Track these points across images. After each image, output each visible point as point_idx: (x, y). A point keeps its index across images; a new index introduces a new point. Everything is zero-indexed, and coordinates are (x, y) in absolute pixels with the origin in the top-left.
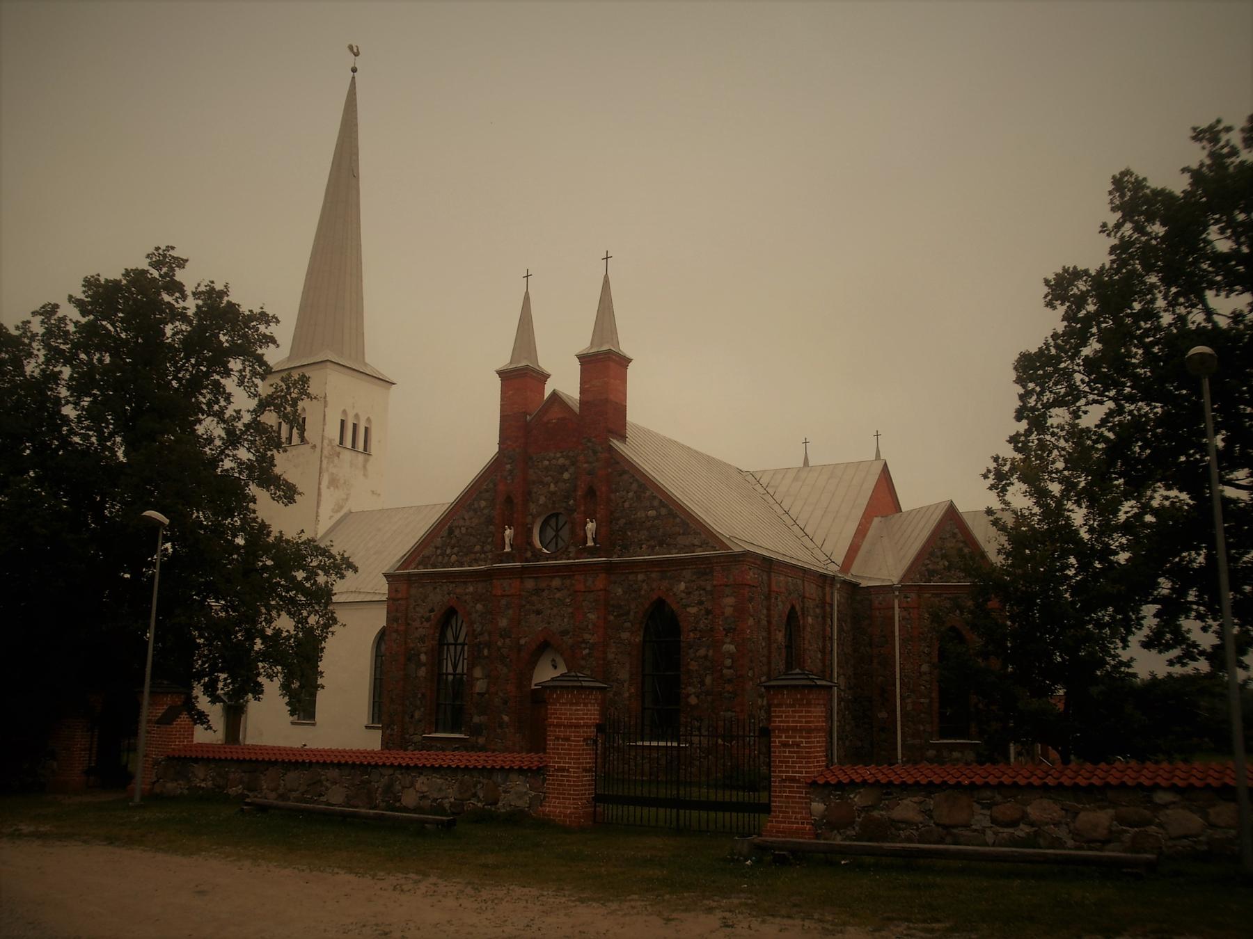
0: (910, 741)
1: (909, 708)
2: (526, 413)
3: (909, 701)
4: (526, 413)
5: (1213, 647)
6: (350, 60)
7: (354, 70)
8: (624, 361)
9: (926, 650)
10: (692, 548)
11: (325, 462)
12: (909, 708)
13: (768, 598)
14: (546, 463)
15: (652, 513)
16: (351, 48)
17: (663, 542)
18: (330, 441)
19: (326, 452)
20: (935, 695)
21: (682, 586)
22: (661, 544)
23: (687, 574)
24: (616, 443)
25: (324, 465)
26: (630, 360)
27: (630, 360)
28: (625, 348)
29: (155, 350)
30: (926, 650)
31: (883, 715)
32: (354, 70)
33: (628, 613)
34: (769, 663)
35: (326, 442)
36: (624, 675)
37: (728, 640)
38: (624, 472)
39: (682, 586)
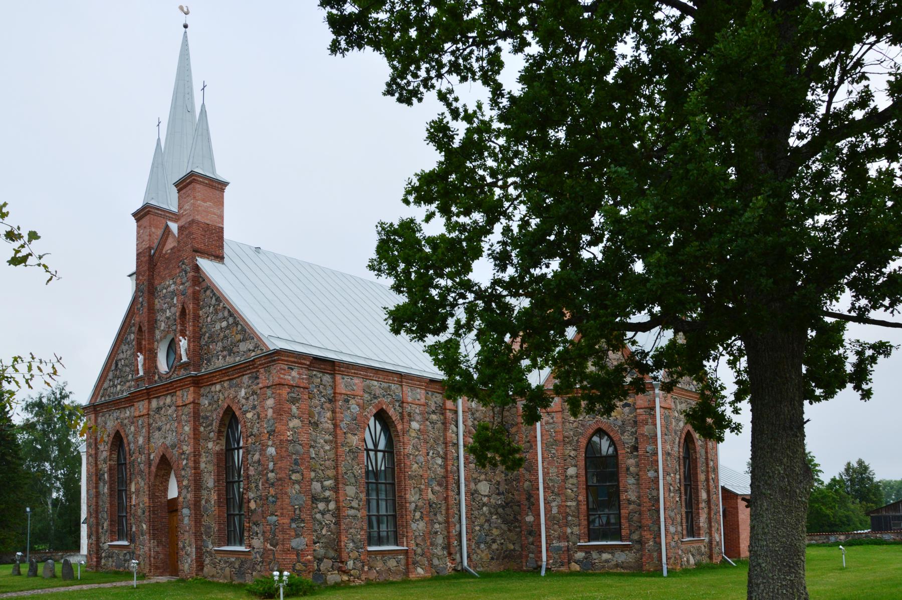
0: (556, 544)
1: (555, 511)
3: (554, 504)
5: (530, 384)
6: (183, 19)
7: (186, 26)
8: (219, 186)
9: (573, 453)
12: (555, 511)
13: (332, 400)
14: (165, 291)
15: (224, 324)
16: (181, 8)
20: (581, 498)
21: (243, 392)
23: (245, 379)
24: (206, 265)
26: (225, 184)
27: (225, 184)
30: (573, 453)
31: (530, 518)
32: (186, 26)
33: (211, 424)
34: (336, 468)
36: (211, 484)
37: (270, 443)
38: (208, 288)
39: (243, 392)
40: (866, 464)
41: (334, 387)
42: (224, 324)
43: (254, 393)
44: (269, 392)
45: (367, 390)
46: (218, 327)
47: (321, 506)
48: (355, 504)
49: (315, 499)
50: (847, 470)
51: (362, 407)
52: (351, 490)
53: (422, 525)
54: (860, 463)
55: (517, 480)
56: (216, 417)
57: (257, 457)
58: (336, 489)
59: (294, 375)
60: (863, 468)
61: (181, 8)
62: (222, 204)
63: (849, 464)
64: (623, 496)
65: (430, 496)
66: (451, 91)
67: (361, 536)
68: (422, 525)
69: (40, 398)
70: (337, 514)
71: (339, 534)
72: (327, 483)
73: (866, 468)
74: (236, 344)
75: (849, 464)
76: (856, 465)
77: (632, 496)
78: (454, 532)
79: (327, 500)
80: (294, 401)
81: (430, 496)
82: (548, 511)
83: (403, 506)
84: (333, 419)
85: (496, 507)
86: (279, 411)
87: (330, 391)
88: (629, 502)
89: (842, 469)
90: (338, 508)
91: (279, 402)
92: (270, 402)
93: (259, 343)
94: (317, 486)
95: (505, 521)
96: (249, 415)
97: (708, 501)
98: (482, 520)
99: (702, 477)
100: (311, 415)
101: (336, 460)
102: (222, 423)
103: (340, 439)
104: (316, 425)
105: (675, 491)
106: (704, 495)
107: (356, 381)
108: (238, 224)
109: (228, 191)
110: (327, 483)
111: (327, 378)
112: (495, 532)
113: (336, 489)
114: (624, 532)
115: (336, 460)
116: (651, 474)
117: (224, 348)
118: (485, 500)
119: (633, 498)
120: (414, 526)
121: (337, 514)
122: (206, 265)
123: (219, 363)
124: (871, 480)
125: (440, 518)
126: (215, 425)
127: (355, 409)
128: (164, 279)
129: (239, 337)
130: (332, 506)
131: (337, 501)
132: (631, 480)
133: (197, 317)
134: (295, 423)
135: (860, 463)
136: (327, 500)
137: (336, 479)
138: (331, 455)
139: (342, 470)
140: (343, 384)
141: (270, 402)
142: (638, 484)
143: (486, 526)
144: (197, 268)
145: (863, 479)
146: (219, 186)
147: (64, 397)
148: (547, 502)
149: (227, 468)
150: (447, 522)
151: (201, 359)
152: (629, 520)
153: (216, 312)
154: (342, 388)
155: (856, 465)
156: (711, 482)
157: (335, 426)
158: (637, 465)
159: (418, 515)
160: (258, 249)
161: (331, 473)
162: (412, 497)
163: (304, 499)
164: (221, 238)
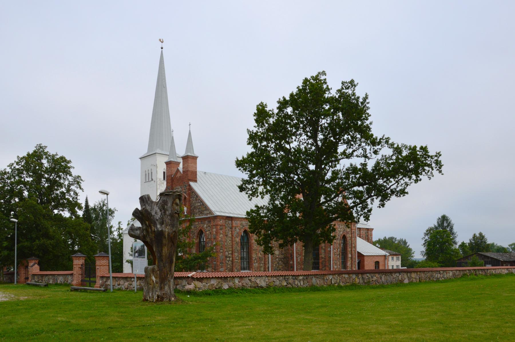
1: (299, 260)
2: (172, 175)
4: (172, 175)
6: (160, 45)
7: (162, 48)
8: (195, 158)
10: (207, 214)
11: (158, 186)
12: (299, 260)
13: (231, 228)
15: (199, 204)
16: (160, 40)
17: (201, 213)
18: (160, 179)
19: (158, 183)
21: (205, 226)
22: (201, 213)
23: (206, 222)
24: (192, 184)
25: (158, 187)
28: (196, 153)
29: (45, 171)
31: (291, 262)
32: (162, 48)
34: (232, 248)
35: (158, 179)
38: (193, 192)
39: (205, 226)
40: (483, 234)
41: (232, 224)
42: (199, 204)
43: (209, 226)
44: (214, 227)
45: (241, 224)
46: (197, 205)
47: (228, 259)
48: (237, 258)
49: (226, 257)
50: (474, 237)
51: (240, 230)
52: (236, 254)
53: (257, 264)
54: (481, 234)
55: (288, 250)
56: (196, 232)
57: (210, 245)
58: (232, 254)
59: (221, 222)
60: (482, 236)
61: (160, 40)
62: (196, 163)
63: (475, 235)
64: (320, 256)
65: (260, 255)
66: (262, 198)
67: (239, 268)
68: (257, 264)
69: (95, 206)
70: (232, 261)
71: (233, 267)
72: (230, 252)
73: (483, 237)
74: (203, 211)
75: (475, 235)
76: (478, 235)
77: (323, 256)
78: (267, 267)
79: (229, 257)
80: (221, 229)
81: (260, 255)
82: (297, 260)
83: (251, 259)
84: (232, 233)
85: (281, 258)
86: (217, 232)
87: (231, 226)
88: (322, 258)
89: (471, 237)
90: (233, 260)
91: (217, 230)
92: (214, 230)
93: (211, 212)
94: (227, 253)
95: (284, 263)
96: (208, 233)
97: (352, 258)
98: (276, 262)
99: (349, 250)
100: (225, 233)
101: (232, 246)
102: (198, 234)
103: (234, 239)
104: (227, 236)
105: (337, 255)
106: (350, 256)
107: (238, 222)
108: (201, 167)
109: (198, 160)
110: (230, 252)
111: (230, 222)
112: (280, 267)
113: (232, 254)
114: (320, 268)
115: (232, 246)
116: (329, 249)
117: (199, 211)
118: (277, 256)
119: (323, 257)
120: (254, 265)
121: (232, 261)
122: (192, 184)
123: (197, 217)
124: (485, 242)
125: (263, 262)
126: (196, 234)
127: (238, 230)
128: (177, 186)
129: (204, 209)
130: (231, 259)
131: (232, 257)
132: (323, 251)
133: (190, 201)
134: (221, 235)
135: (481, 234)
136: (229, 257)
137: (232, 251)
138: (231, 244)
139: (234, 248)
140: (235, 223)
141: (214, 230)
142: (325, 252)
143: (277, 265)
144: (190, 185)
145: (482, 242)
146: (195, 158)
147: (104, 205)
148: (297, 257)
149: (199, 247)
150: (265, 263)
151: (191, 214)
152: (322, 264)
153: (196, 200)
154: (234, 225)
155: (478, 235)
156: (353, 251)
157: (232, 235)
158: (325, 246)
159: (256, 261)
160: (205, 173)
161: (231, 249)
162: (254, 256)
163: (224, 257)
164: (196, 175)
